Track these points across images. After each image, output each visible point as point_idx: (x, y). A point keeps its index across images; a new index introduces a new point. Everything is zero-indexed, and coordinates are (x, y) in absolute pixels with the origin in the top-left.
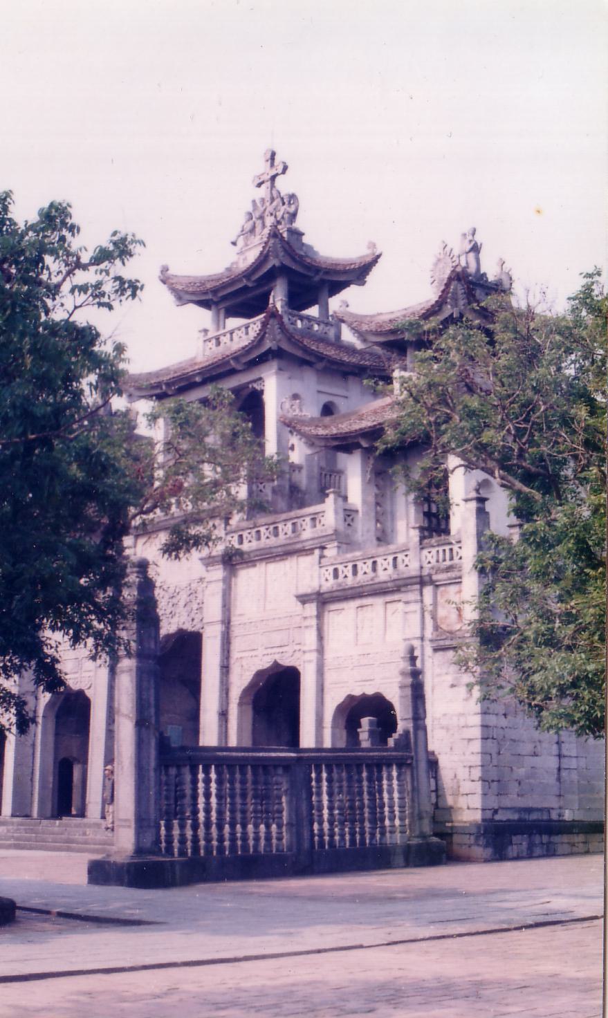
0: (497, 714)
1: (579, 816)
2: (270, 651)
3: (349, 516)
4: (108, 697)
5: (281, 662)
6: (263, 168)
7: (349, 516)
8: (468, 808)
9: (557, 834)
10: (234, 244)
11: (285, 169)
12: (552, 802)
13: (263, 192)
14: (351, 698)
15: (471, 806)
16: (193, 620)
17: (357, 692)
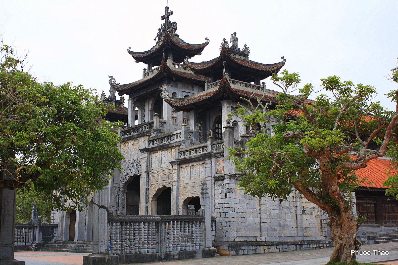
1: (268, 239)
2: (162, 182)
4: (146, 196)
6: (163, 13)
8: (226, 237)
9: (259, 246)
10: (155, 40)
12: (257, 234)
13: (164, 22)
14: (188, 198)
15: (226, 236)
16: (139, 171)
17: (190, 196)
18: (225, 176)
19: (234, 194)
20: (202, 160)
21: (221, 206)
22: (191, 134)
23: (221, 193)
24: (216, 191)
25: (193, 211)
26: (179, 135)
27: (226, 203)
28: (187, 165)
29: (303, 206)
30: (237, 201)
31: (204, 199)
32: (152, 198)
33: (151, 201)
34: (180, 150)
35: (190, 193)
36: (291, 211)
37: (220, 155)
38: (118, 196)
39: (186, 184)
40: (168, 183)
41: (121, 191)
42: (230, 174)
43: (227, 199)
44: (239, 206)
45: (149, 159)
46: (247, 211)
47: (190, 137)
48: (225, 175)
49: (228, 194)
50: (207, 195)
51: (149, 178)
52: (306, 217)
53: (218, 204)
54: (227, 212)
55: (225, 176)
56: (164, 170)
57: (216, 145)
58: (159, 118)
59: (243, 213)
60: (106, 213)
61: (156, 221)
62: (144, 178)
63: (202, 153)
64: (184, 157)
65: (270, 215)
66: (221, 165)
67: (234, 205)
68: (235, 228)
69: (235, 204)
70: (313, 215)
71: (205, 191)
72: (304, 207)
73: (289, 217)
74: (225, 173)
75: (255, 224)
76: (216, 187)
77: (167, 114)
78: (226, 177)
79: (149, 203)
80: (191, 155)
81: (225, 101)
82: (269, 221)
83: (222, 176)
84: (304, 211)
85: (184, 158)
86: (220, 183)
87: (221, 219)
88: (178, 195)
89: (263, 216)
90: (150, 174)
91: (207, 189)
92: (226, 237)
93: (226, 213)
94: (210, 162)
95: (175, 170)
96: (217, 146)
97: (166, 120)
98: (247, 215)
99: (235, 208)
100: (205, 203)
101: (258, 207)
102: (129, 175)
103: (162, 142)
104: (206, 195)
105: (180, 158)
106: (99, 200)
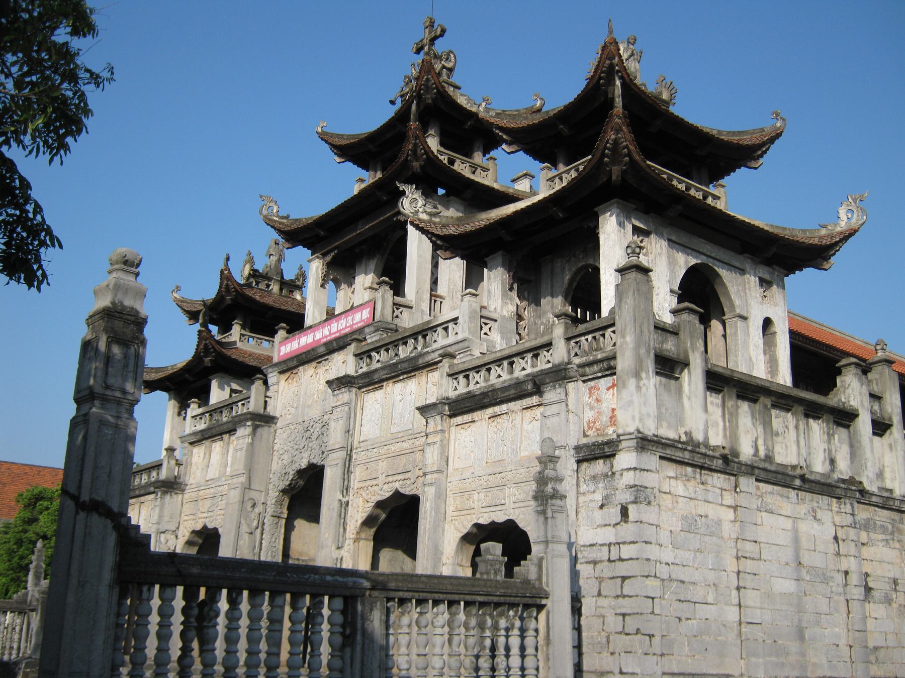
0: (654, 654)
2: (390, 479)
3: (486, 324)
5: (402, 491)
7: (486, 324)
8: (621, 673)
10: (393, 102)
11: (443, 31)
15: (624, 670)
18: (620, 441)
19: (653, 509)
20: (530, 395)
21: (604, 554)
22: (491, 323)
23: (602, 507)
24: (582, 499)
25: (497, 567)
26: (451, 325)
27: (624, 543)
28: (477, 415)
29: (864, 572)
30: (664, 537)
31: (546, 518)
32: (357, 533)
33: (351, 542)
34: (455, 368)
35: (485, 510)
36: (831, 587)
37: (600, 371)
38: (259, 531)
39: (470, 480)
40: (408, 482)
41: (270, 514)
42: (639, 432)
43: (630, 525)
44: (668, 555)
45: (355, 409)
46: (697, 576)
47: (486, 334)
48: (622, 438)
49: (632, 509)
50: (558, 502)
51: (352, 469)
52: (876, 610)
53: (591, 545)
54: (629, 577)
55: (620, 441)
56: (397, 440)
57: (583, 338)
58: (392, 292)
59: (682, 582)
60: (112, 539)
61: (347, 593)
62: (334, 469)
63: (529, 370)
64: (465, 390)
65: (769, 596)
66: (604, 405)
67: (653, 552)
68: (657, 640)
69: (658, 547)
70: (895, 605)
71: (550, 486)
72: (867, 575)
73: (826, 610)
74: (620, 431)
75: (722, 629)
76: (582, 484)
77: (418, 283)
78: (624, 444)
79: (346, 548)
80: (490, 383)
81: (611, 205)
82: (767, 617)
83: (609, 443)
84: (868, 589)
85: (469, 392)
86: (599, 466)
87: (602, 602)
88: (441, 517)
89: (751, 598)
90: (354, 456)
91: (560, 480)
92: (621, 673)
93: (624, 578)
94: (563, 397)
95: (436, 432)
96: (587, 340)
97: (414, 301)
98: (697, 594)
99: (658, 564)
100: (549, 535)
101: (731, 565)
102: (296, 467)
103: (396, 355)
104: (554, 501)
105: (452, 394)
106: (81, 475)
